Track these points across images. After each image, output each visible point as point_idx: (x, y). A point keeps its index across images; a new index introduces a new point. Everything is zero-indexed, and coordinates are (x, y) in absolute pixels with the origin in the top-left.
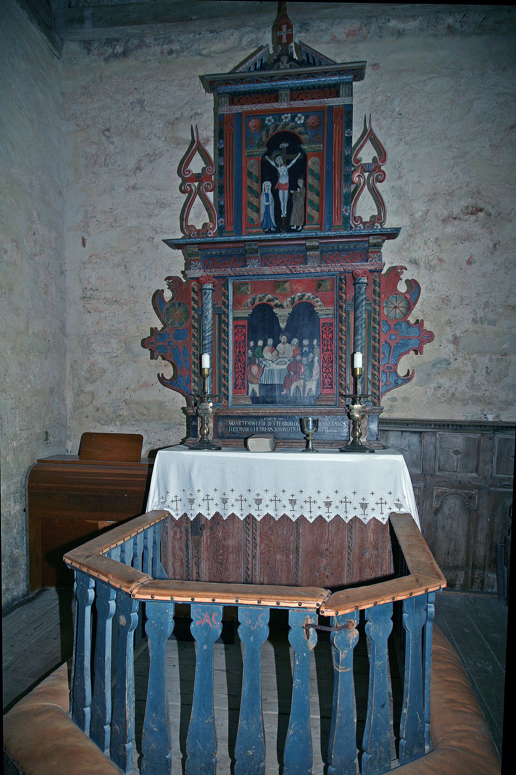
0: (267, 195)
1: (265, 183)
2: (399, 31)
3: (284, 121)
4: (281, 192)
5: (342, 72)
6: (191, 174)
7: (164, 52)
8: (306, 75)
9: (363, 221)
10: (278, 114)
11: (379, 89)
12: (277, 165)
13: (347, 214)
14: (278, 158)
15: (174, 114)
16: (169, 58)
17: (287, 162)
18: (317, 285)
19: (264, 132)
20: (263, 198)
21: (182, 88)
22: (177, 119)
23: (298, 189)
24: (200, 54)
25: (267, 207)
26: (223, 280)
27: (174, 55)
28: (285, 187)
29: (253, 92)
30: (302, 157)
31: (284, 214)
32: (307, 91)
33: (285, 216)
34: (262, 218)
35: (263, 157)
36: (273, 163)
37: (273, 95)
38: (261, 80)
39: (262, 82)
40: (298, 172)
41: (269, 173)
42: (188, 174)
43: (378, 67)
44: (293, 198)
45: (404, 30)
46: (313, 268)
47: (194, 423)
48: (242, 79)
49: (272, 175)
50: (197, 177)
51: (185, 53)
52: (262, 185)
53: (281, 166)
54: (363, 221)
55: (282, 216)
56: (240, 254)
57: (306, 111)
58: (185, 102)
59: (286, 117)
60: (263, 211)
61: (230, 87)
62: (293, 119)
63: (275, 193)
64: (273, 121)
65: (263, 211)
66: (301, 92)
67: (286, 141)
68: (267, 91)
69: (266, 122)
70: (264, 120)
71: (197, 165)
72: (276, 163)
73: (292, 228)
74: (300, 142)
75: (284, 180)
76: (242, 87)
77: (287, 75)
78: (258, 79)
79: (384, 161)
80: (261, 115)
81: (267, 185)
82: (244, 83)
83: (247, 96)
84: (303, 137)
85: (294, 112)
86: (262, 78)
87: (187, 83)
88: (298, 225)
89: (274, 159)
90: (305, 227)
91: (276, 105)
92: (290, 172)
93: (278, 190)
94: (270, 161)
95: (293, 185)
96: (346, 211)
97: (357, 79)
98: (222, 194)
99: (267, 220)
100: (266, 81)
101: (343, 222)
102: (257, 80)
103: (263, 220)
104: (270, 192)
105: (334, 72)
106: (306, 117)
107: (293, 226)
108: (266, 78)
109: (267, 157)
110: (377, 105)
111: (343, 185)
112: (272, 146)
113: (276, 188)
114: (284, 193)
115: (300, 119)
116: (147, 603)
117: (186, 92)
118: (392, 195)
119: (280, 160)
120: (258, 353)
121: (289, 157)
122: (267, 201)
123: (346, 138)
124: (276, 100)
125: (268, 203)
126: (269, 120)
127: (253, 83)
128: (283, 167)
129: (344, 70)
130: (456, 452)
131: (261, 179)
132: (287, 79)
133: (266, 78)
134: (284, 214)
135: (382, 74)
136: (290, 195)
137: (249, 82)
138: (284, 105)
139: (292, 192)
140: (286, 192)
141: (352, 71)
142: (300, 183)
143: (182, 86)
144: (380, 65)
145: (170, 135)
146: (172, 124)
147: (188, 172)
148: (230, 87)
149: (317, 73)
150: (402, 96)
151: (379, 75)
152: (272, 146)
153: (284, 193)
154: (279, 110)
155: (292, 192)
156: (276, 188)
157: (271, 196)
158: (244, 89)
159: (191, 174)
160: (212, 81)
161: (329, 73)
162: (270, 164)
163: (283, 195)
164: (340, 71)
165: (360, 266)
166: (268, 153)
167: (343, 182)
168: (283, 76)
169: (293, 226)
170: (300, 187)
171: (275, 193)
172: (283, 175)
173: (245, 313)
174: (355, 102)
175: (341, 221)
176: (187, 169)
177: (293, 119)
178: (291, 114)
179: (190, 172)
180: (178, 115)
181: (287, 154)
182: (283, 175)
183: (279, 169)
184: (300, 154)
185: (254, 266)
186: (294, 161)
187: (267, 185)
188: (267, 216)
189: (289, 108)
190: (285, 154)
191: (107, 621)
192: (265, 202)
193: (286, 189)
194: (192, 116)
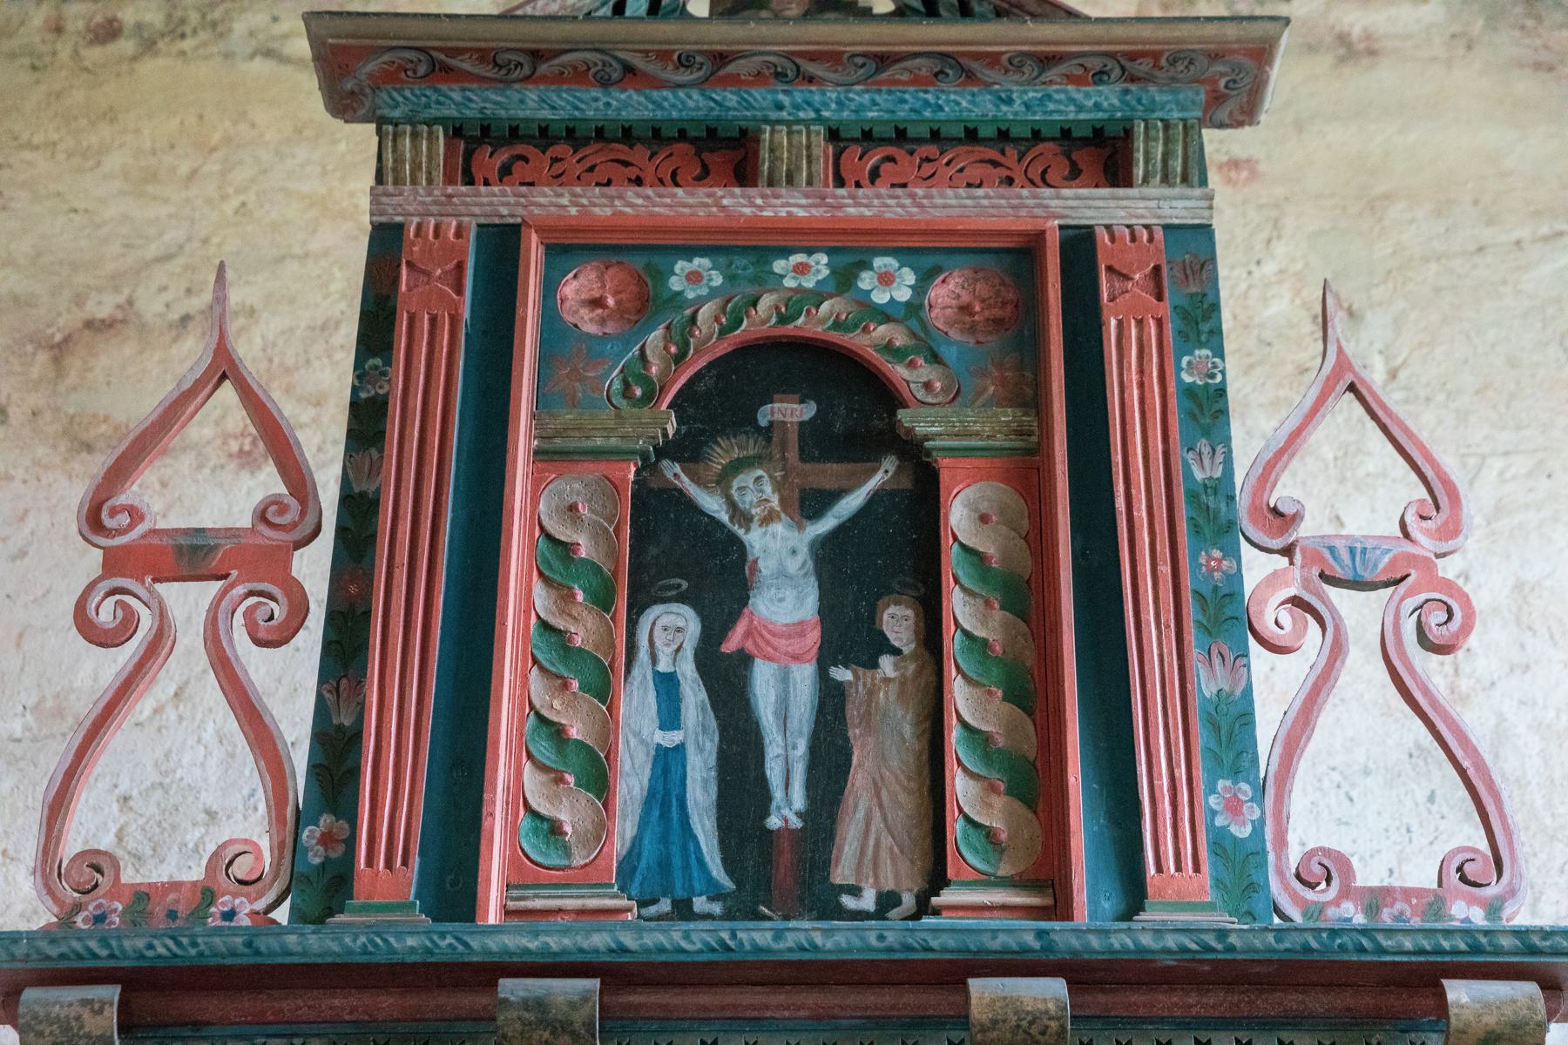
0: (667, 685)
1: (656, 610)
2: (1343, 39)
3: (789, 283)
4: (764, 682)
5: (1143, 66)
6: (141, 529)
7: (70, 27)
8: (925, 67)
9: (1360, 881)
10: (753, 248)
11: (1270, 268)
12: (745, 519)
13: (1243, 832)
14: (746, 479)
15: (79, 300)
16: (94, 54)
17: (811, 504)
19: (655, 337)
20: (637, 704)
21: (150, 189)
22: (97, 327)
23: (886, 662)
24: (268, 53)
25: (668, 763)
27: (126, 46)
28: (795, 646)
29: (600, 132)
30: (906, 483)
31: (787, 807)
32: (931, 150)
33: (796, 823)
34: (624, 829)
35: (648, 466)
36: (712, 504)
38: (652, 68)
39: (661, 85)
40: (884, 562)
41: (684, 557)
42: (131, 527)
43: (1254, 175)
44: (852, 712)
45: (1368, 36)
48: (537, 56)
49: (708, 570)
50: (192, 556)
51: (187, 44)
52: (632, 624)
53: (768, 519)
54: (1360, 881)
55: (774, 822)
57: (927, 250)
58: (152, 250)
59: (801, 269)
60: (632, 780)
61: (457, 96)
62: (844, 279)
63: (726, 678)
64: (718, 280)
65: (632, 780)
66: (891, 150)
68: (682, 134)
69: (675, 284)
70: (662, 275)
71: (211, 488)
72: (732, 506)
73: (848, 901)
74: (888, 397)
75: (785, 599)
76: (532, 103)
77: (813, 57)
78: (638, 61)
79: (1452, 530)
80: (640, 256)
81: (673, 628)
82: (544, 79)
83: (561, 149)
84: (908, 376)
85: (852, 250)
86: (664, 56)
87: (184, 169)
88: (889, 885)
89: (722, 482)
90: (947, 897)
91: (740, 204)
92: (832, 559)
93: (744, 660)
94: (692, 490)
95: (847, 636)
96: (1234, 807)
97: (1222, 114)
98: (346, 666)
99: (664, 838)
100: (684, 77)
101: (1218, 883)
102: (629, 69)
103: (637, 841)
104: (687, 670)
105: (1095, 64)
106: (925, 279)
107: (855, 891)
108: (685, 62)
109: (673, 471)
110: (1268, 335)
111: (1194, 653)
112: (721, 401)
113: (730, 645)
114: (785, 678)
115: (886, 279)
117: (164, 211)
118: (1421, 796)
119: (757, 489)
121: (827, 474)
122: (670, 717)
123: (1190, 392)
124: (744, 174)
125: (675, 737)
126: (694, 279)
127: (605, 83)
128: (778, 528)
129: (1156, 55)
131: (634, 589)
132: (811, 80)
133: (685, 62)
134: (787, 807)
135: (1276, 206)
136: (831, 700)
137: (579, 76)
138: (792, 206)
139: (842, 674)
140: (804, 676)
141: (1202, 62)
142: (898, 623)
143: (151, 177)
144: (1262, 167)
145: (35, 400)
146: (60, 350)
147: (124, 519)
148: (457, 96)
149: (993, 60)
150: (1401, 305)
151: (1261, 207)
153: (785, 678)
154: (759, 228)
155: (842, 674)
156: (730, 645)
157: (694, 695)
158: (546, 114)
159: (141, 529)
160: (344, 49)
161: (1063, 68)
162: (692, 507)
163: (783, 693)
164: (1133, 56)
166: (687, 449)
167: (1192, 634)
168: (788, 56)
169: (855, 891)
170: (896, 652)
171: (726, 678)
172: (782, 573)
174: (1232, 217)
175: (1206, 867)
176: (122, 499)
177: (844, 279)
179: (136, 515)
180: (103, 307)
181: (804, 456)
182: (782, 573)
183: (753, 538)
184: (889, 464)
186: (852, 502)
187: (673, 628)
188: (664, 816)
190: (793, 455)
193: (796, 658)
194: (186, 319)
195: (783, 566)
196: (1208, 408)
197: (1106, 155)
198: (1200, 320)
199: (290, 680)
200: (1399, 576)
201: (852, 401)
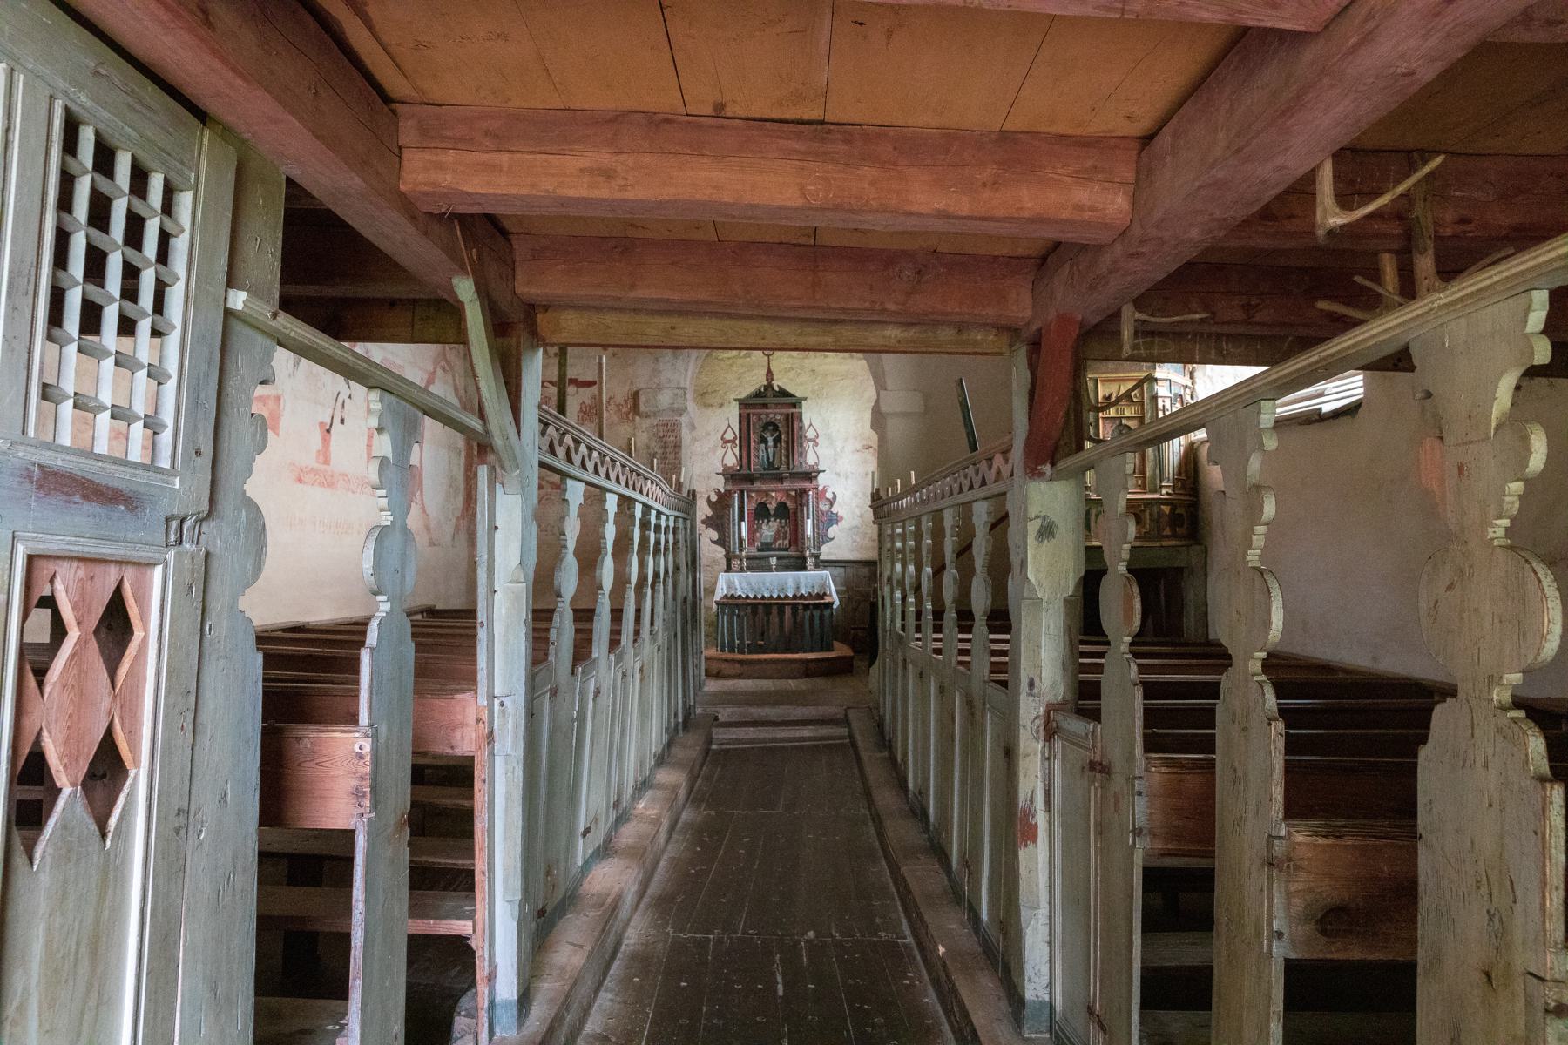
18: (787, 493)
26: (742, 492)
37: (765, 406)
40: (777, 440)
41: (764, 440)
46: (786, 485)
47: (773, 562)
49: (765, 441)
56: (750, 479)
67: (772, 426)
71: (729, 436)
75: (771, 444)
112: (765, 427)
116: (19, 797)
120: (760, 527)
130: (1138, 832)
152: (765, 427)
163: (771, 451)
165: (806, 485)
173: (753, 506)
178: (776, 415)
185: (757, 485)
189: (1015, 814)
191: (1273, 512)
192: (762, 454)
195: (770, 439)
196: (801, 428)
197: (794, 405)
199: (737, 450)
201: (776, 428)
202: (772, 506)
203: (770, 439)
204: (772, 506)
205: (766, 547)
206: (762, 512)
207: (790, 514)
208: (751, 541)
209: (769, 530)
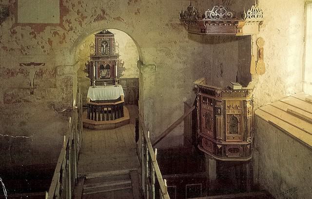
40: (107, 46)
75: (105, 47)
112: (103, 42)
163: (105, 49)
178: (106, 38)
195: (104, 46)
196: (114, 43)
198: (114, 40)
200: (39, 62)
201: (106, 42)
202: (105, 66)
203: (104, 46)
204: (105, 66)
205: (103, 78)
206: (102, 67)
207: (111, 68)
208: (99, 77)
209: (104, 73)
